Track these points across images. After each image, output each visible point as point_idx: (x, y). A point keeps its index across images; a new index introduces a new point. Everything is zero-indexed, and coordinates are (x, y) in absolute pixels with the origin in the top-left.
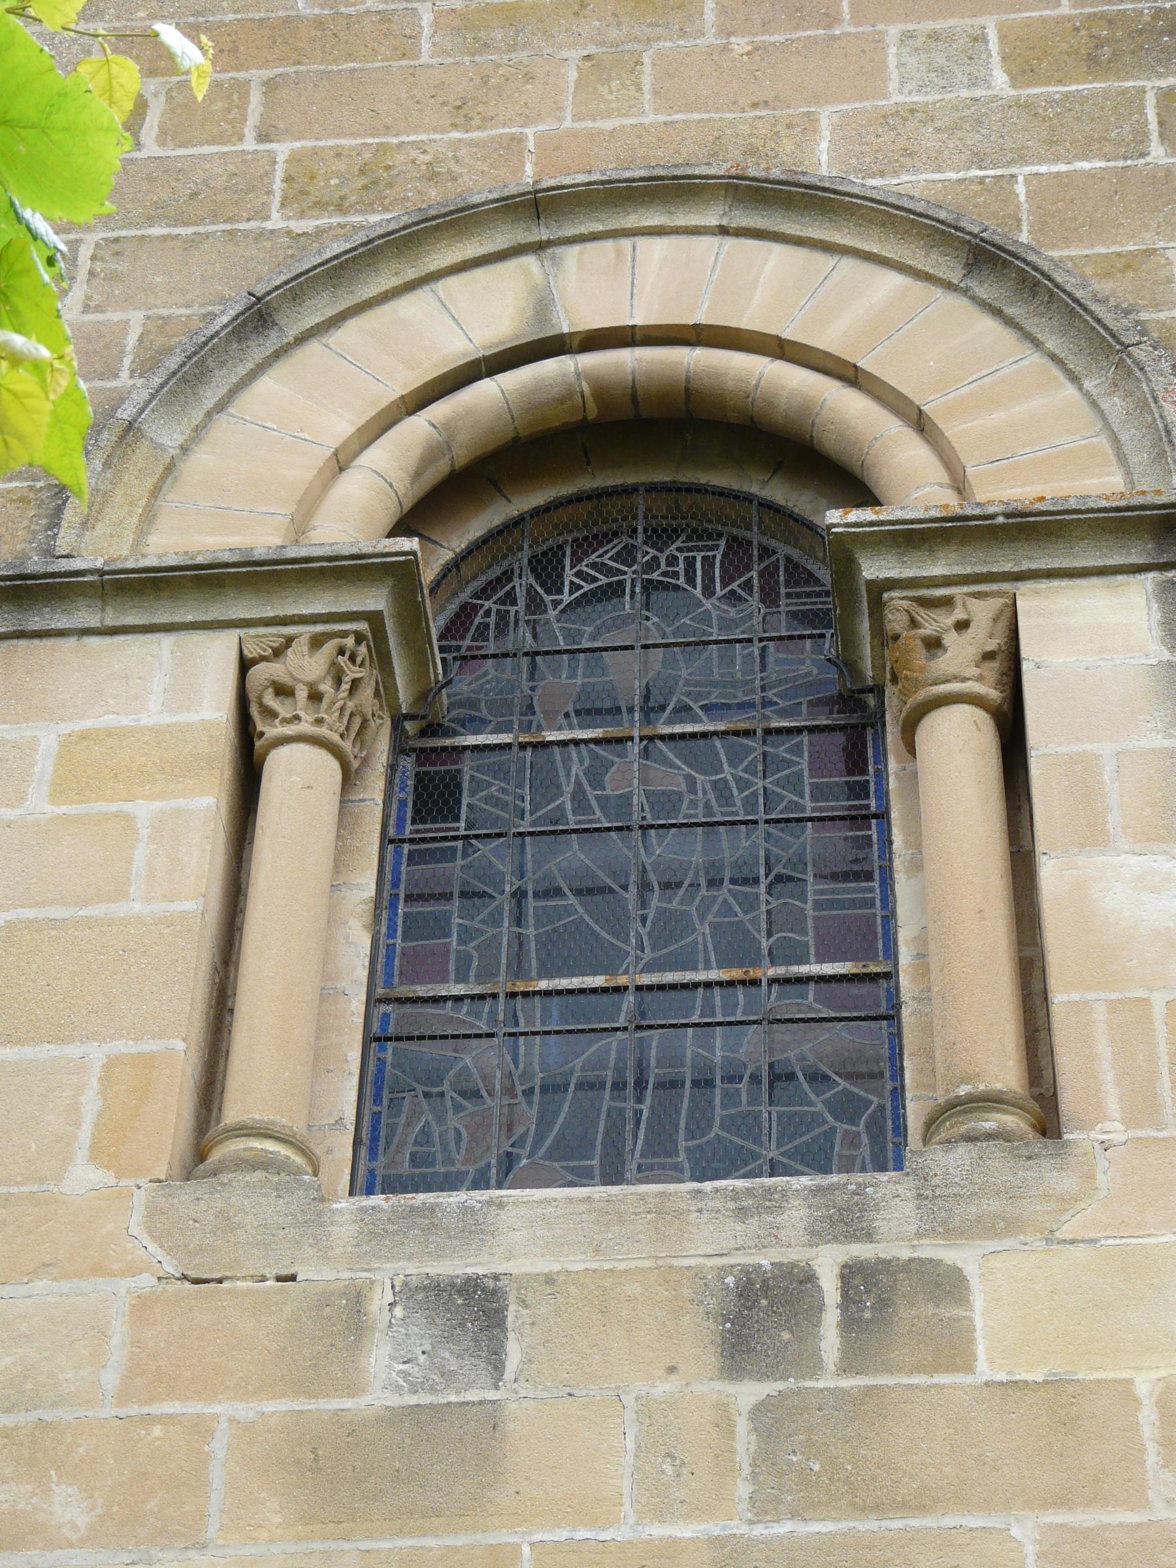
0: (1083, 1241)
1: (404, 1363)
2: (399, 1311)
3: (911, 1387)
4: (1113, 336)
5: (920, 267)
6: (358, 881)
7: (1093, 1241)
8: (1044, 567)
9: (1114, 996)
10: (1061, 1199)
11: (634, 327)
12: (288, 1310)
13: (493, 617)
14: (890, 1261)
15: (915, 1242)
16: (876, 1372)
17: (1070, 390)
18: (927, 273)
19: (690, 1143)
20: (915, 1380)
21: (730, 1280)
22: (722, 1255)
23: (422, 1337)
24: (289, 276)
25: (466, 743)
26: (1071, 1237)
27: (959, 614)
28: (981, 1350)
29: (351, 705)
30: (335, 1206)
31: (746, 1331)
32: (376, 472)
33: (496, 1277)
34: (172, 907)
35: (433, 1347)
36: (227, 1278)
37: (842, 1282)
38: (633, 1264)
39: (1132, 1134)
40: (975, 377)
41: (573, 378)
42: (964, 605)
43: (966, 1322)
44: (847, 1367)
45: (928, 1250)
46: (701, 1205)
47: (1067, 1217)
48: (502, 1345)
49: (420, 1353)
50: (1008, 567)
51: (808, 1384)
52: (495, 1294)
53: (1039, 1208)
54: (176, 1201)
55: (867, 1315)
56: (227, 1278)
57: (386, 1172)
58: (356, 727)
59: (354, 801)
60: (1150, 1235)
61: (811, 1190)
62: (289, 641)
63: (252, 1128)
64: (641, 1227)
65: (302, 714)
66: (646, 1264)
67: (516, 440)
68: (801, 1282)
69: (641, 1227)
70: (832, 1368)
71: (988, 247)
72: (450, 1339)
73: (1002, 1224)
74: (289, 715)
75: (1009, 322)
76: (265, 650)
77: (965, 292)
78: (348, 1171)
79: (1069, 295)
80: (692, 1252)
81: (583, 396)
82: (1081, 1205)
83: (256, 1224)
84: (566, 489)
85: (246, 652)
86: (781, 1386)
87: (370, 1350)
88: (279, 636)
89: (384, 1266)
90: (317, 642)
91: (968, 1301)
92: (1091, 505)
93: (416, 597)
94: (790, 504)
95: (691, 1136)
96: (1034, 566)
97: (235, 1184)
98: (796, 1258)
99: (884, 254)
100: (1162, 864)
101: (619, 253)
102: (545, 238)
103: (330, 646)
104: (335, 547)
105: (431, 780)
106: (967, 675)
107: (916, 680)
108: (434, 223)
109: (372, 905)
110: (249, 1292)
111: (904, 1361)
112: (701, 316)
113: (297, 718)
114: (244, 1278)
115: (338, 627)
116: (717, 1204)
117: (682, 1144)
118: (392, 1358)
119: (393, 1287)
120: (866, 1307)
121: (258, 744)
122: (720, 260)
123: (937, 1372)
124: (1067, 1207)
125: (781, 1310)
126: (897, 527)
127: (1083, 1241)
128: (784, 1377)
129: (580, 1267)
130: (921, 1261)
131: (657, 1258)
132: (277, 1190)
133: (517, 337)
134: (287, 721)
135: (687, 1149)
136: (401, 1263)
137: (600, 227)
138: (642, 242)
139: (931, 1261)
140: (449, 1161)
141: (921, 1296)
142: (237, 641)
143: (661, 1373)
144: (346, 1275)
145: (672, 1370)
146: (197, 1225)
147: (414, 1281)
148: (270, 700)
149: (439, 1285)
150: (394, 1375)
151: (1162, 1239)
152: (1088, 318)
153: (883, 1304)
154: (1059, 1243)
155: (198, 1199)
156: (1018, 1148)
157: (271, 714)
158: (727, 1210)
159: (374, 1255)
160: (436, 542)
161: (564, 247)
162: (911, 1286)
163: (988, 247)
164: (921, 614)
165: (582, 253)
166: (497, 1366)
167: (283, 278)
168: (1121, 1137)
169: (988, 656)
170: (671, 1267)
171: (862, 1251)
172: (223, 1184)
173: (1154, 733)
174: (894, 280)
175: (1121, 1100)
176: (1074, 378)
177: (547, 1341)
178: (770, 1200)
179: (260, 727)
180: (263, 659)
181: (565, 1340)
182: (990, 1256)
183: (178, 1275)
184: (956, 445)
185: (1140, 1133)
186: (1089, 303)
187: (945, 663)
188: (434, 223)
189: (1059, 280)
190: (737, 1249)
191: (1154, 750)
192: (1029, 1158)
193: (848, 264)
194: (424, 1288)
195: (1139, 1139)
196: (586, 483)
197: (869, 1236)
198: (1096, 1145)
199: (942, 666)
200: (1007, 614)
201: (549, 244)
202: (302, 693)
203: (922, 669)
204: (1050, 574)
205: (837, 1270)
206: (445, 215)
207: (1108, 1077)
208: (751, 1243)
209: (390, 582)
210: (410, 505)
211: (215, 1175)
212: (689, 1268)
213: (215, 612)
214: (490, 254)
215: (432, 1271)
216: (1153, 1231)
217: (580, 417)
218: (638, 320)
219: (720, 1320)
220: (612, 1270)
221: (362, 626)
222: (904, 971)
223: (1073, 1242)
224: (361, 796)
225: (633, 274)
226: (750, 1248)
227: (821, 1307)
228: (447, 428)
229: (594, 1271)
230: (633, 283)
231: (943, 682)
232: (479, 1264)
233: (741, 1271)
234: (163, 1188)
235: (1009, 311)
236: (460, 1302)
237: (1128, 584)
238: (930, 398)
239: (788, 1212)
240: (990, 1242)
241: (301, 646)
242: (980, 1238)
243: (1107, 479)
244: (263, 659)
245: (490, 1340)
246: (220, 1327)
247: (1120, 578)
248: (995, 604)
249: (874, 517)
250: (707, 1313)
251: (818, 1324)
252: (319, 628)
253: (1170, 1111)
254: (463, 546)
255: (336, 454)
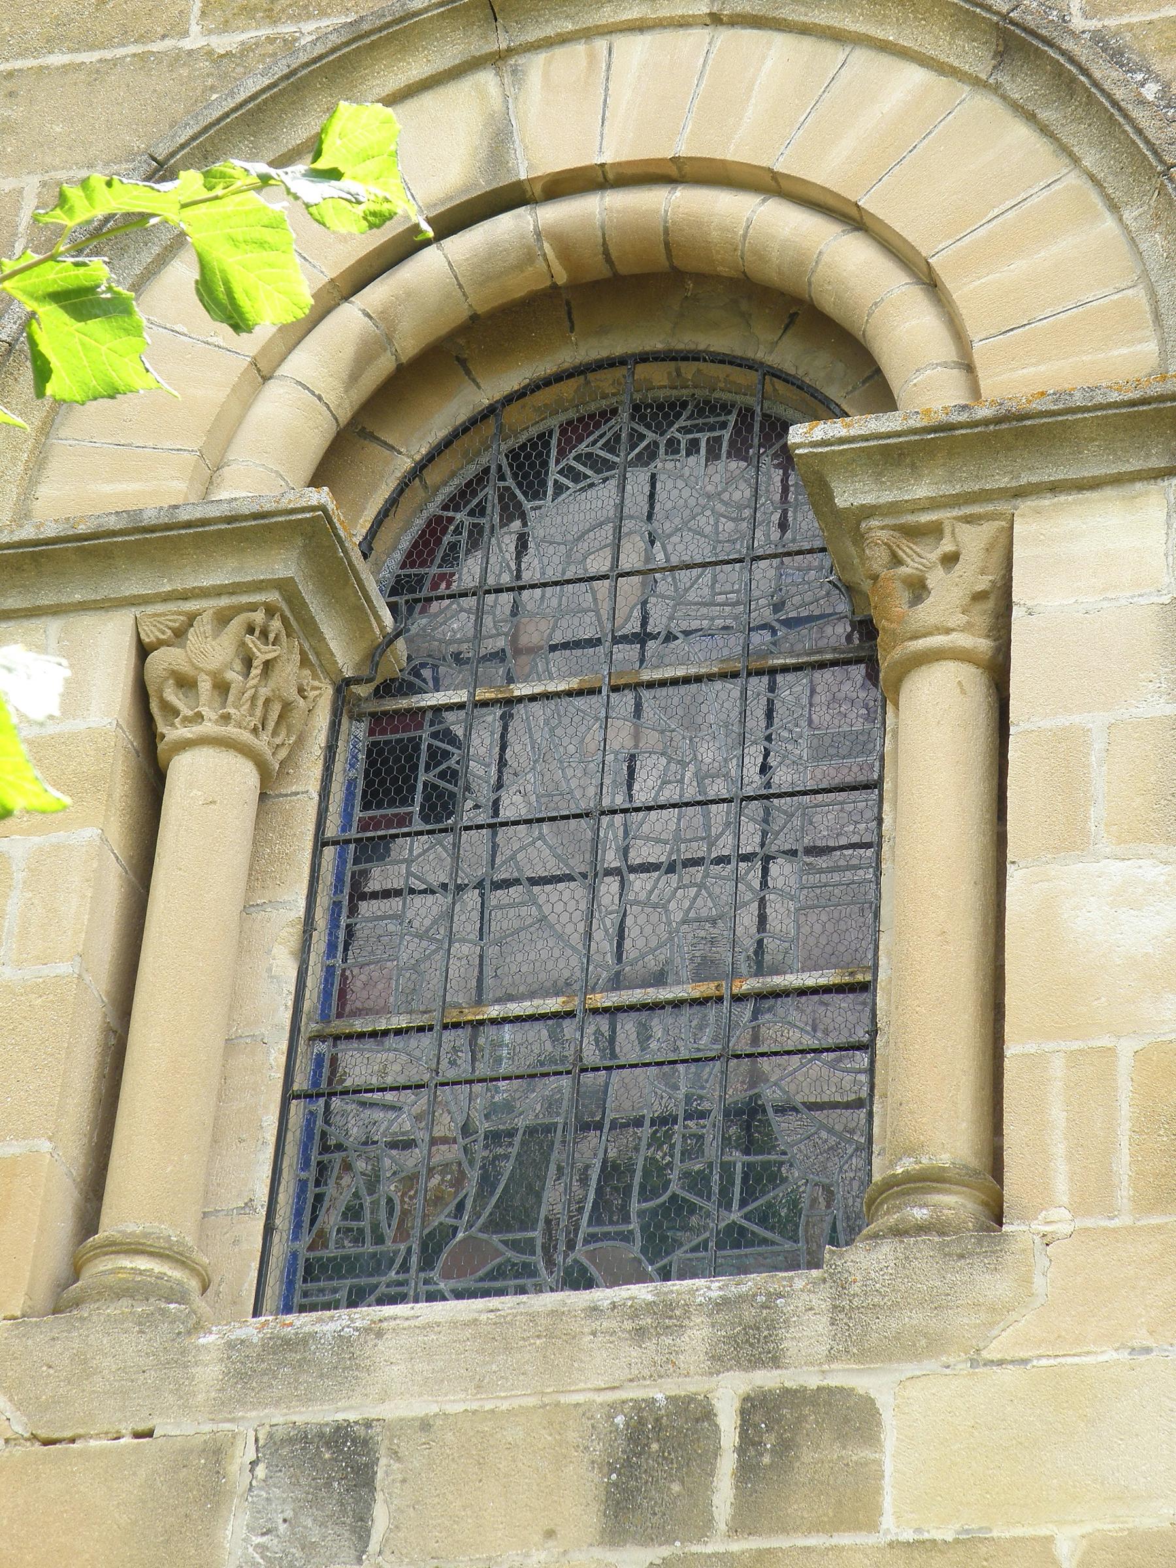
0: (1012, 1362)
1: (263, 1534)
2: (261, 1471)
3: (807, 1549)
4: (1155, 153)
5: (943, 58)
6: (286, 897)
7: (1024, 1362)
8: (1046, 478)
9: (1076, 1045)
10: (992, 1309)
11: (602, 165)
12: (142, 1473)
13: (465, 534)
14: (796, 1391)
15: (826, 1367)
16: (772, 1531)
17: (1109, 223)
18: (951, 66)
19: (644, 1205)
20: (812, 1541)
21: (620, 1420)
22: (614, 1388)
23: (284, 1501)
24: (197, 129)
25: (423, 704)
26: (999, 1356)
27: (947, 546)
28: (888, 1501)
29: (264, 692)
30: (202, 1341)
31: (633, 1483)
32: (300, 383)
33: (368, 1424)
34: (46, 971)
35: (296, 1514)
36: (80, 1437)
37: (743, 1419)
38: (516, 1403)
39: (1080, 1223)
40: (996, 212)
41: (531, 239)
42: (953, 533)
43: (874, 1467)
44: (738, 1528)
45: (840, 1377)
46: (595, 1325)
47: (996, 1332)
48: (369, 1507)
49: (281, 1521)
50: (1004, 482)
51: (695, 1548)
52: (365, 1445)
53: (966, 1320)
54: (30, 1342)
55: (766, 1460)
56: (80, 1437)
57: (311, 1255)
58: (274, 715)
59: (286, 795)
60: (1088, 1353)
61: (717, 1304)
62: (191, 618)
63: (121, 1244)
64: (527, 1356)
65: (205, 710)
66: (531, 1401)
67: (474, 318)
68: (697, 1420)
69: (527, 1356)
70: (722, 1527)
71: (1018, 31)
72: (315, 1502)
73: (923, 1342)
74: (190, 713)
75: (1044, 130)
76: (163, 633)
77: (996, 89)
78: (255, 1265)
79: (1109, 96)
80: (582, 1385)
81: (546, 260)
82: (1014, 1315)
83: (114, 1368)
84: (545, 367)
85: (143, 636)
86: (665, 1551)
87: (227, 1521)
88: (180, 614)
89: (248, 1415)
90: (223, 619)
91: (879, 1440)
92: (1100, 399)
93: (336, 551)
94: (801, 373)
95: (643, 1197)
96: (1034, 479)
97: (95, 1318)
98: (693, 1390)
99: (901, 42)
100: (1150, 871)
101: (592, 57)
102: (504, 46)
103: (237, 623)
104: (234, 504)
105: (392, 751)
106: (950, 625)
107: (894, 632)
108: (367, 41)
109: (300, 927)
110: (102, 1453)
111: (802, 1518)
112: (682, 148)
113: (199, 717)
114: (98, 1436)
115: (245, 599)
116: (614, 1324)
117: (635, 1206)
118: (251, 1529)
119: (257, 1440)
120: (766, 1450)
121: (161, 747)
122: (710, 62)
123: (837, 1530)
124: (998, 1318)
125: (672, 1456)
126: (872, 443)
127: (1012, 1362)
128: (669, 1541)
129: (459, 1408)
130: (830, 1391)
131: (543, 1394)
132: (140, 1324)
133: (466, 189)
134: (187, 721)
135: (641, 1213)
136: (266, 1411)
137: (569, 26)
138: (622, 43)
139: (841, 1390)
140: (379, 1239)
141: (826, 1436)
142: (132, 622)
143: (537, 1538)
144: (207, 1428)
145: (550, 1534)
146: (51, 1371)
147: (280, 1432)
148: (172, 695)
149: (306, 1437)
150: (251, 1549)
151: (1102, 1358)
152: (1128, 128)
153: (785, 1447)
154: (985, 1365)
155: (53, 1339)
156: (948, 1244)
157: (171, 711)
158: (623, 1331)
159: (238, 1401)
160: (392, 448)
161: (528, 55)
162: (817, 1423)
163: (1018, 31)
164: (906, 549)
165: (548, 63)
166: (361, 1531)
167: (190, 132)
168: (1066, 1228)
169: (978, 597)
170: (558, 1404)
171: (767, 1379)
172: (82, 1319)
173: (1156, 696)
174: (915, 76)
175: (1071, 1179)
176: (1114, 207)
177: (418, 1502)
178: (670, 1318)
179: (162, 728)
180: (161, 643)
181: (437, 1500)
182: (907, 1383)
183: (27, 1435)
184: (963, 311)
185: (1089, 1223)
186: (1130, 107)
187: (927, 613)
188: (367, 41)
189: (1097, 75)
190: (631, 1380)
191: (1152, 719)
192: (961, 1257)
193: (861, 57)
194: (291, 1441)
195: (1087, 1229)
196: (567, 357)
197: (775, 1361)
198: (1037, 1239)
199: (921, 615)
200: (1003, 541)
201: (510, 52)
202: (205, 685)
203: (901, 620)
204: (1054, 488)
205: (737, 1405)
206: (380, 29)
207: (1059, 1149)
208: (646, 1373)
209: (300, 542)
210: (349, 415)
211: (77, 1305)
212: (577, 1405)
213: (107, 590)
214: (440, 74)
215: (299, 1419)
216: (1092, 1348)
217: (548, 283)
218: (608, 157)
219: (605, 1470)
220: (493, 1411)
221: (273, 597)
222: (883, 989)
223: (1001, 1363)
224: (294, 789)
225: (607, 89)
226: (644, 1378)
227: (716, 1451)
228: (385, 321)
229: (474, 1412)
230: (605, 100)
231: (924, 635)
232: (351, 1408)
233: (633, 1408)
234: (17, 1326)
235: (1044, 115)
236: (327, 1456)
237: (1147, 493)
238: (941, 247)
239: (689, 1332)
240: (909, 1366)
241: (204, 624)
242: (899, 1360)
243: (1139, 347)
244: (161, 643)
245: (357, 1503)
246: (67, 1497)
247: (1138, 486)
248: (988, 529)
249: (844, 432)
250: (593, 1462)
251: (712, 1474)
252: (224, 602)
253: (1125, 1194)
254: (424, 451)
255: (254, 363)
